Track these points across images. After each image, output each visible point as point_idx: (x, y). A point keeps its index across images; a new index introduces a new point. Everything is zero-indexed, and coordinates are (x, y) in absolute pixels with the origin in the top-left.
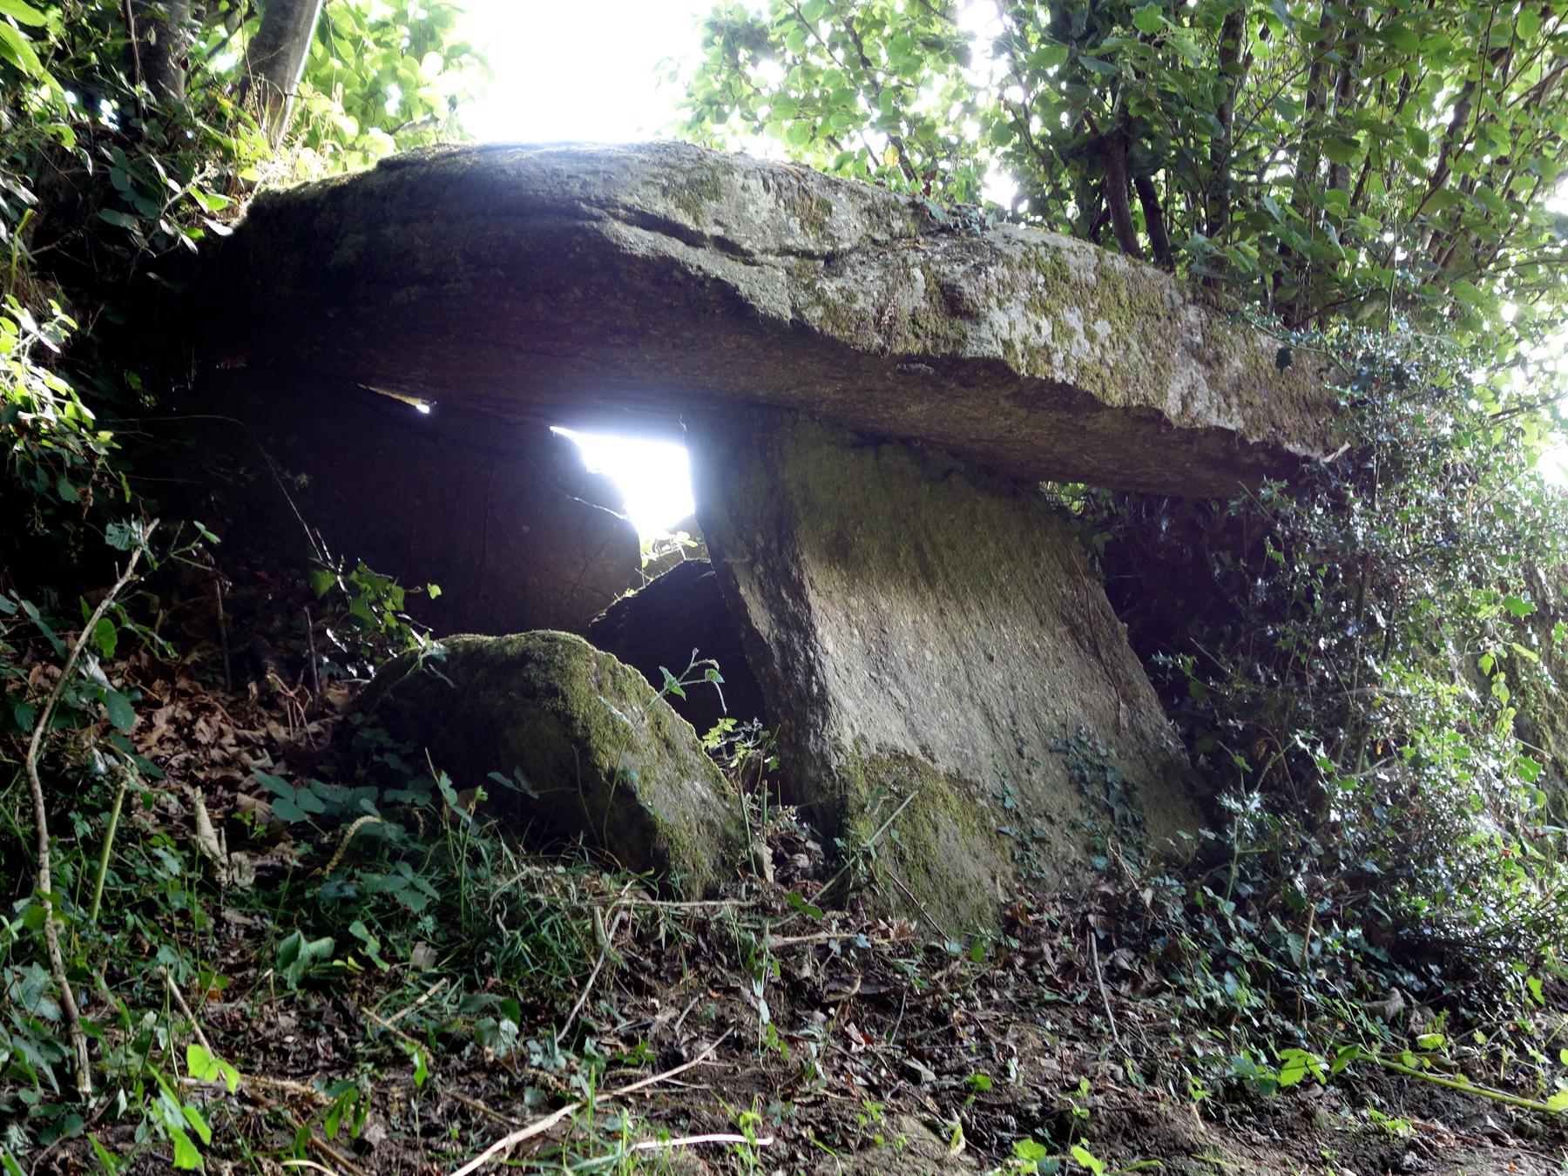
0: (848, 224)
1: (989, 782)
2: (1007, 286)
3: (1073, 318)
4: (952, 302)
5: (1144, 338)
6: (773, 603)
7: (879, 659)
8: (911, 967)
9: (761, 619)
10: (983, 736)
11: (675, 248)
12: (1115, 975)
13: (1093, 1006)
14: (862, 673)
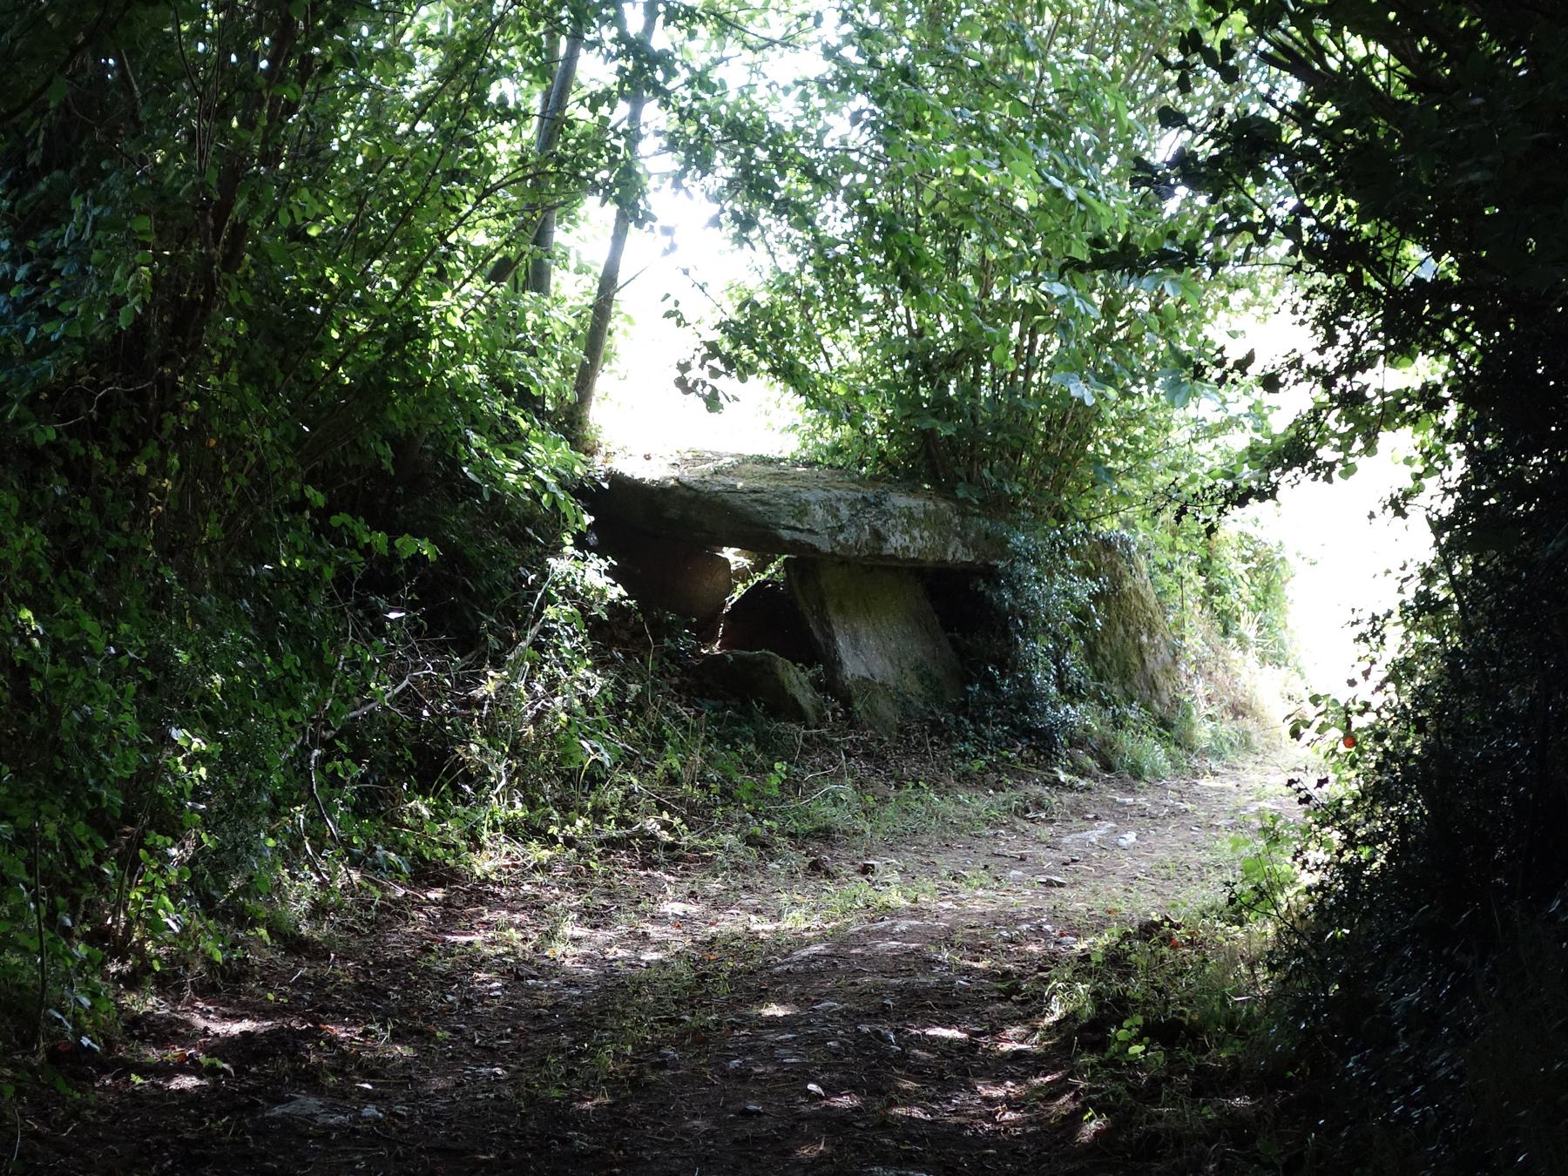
0: (845, 513)
1: (892, 683)
2: (895, 526)
3: (916, 533)
4: (877, 535)
5: (940, 534)
6: (821, 629)
7: (855, 643)
8: (874, 744)
9: (817, 635)
10: (889, 669)
11: (797, 535)
12: (933, 744)
13: (926, 753)
14: (851, 651)
